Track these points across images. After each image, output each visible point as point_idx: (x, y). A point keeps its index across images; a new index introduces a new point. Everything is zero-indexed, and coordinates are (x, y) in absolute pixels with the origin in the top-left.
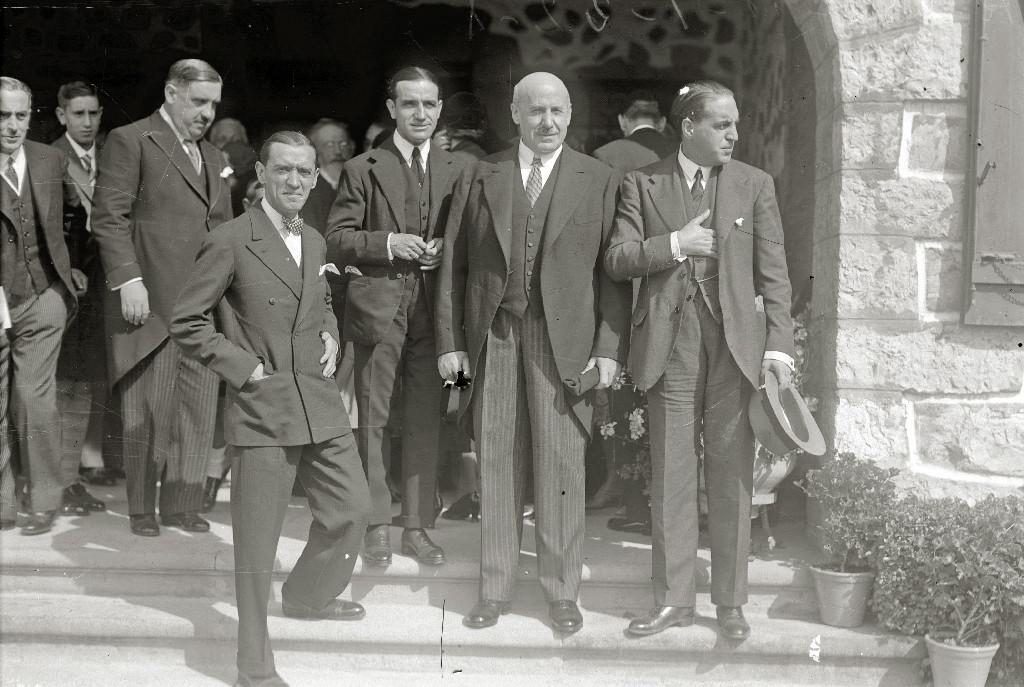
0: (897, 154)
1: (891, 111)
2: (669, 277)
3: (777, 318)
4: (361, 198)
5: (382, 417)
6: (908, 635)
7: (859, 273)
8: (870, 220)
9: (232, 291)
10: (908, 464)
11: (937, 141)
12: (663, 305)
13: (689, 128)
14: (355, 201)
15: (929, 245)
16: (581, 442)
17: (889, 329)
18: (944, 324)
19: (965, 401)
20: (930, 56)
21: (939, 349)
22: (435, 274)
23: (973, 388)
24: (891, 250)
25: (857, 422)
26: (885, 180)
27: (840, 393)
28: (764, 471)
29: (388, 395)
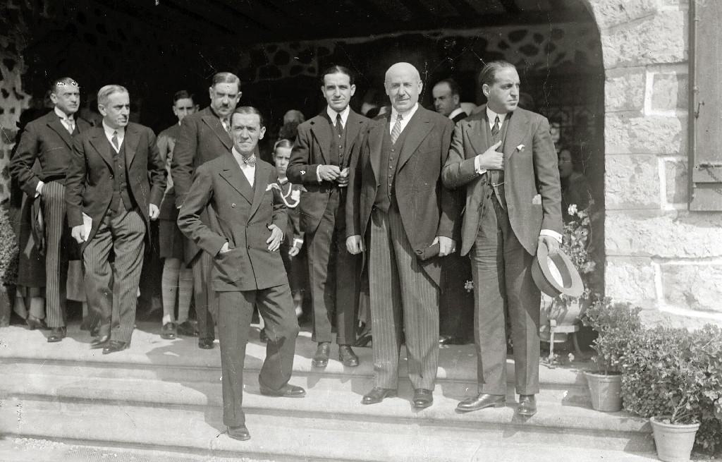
0: (643, 102)
1: (637, 72)
2: (475, 185)
3: (550, 209)
4: (305, 145)
5: (322, 277)
6: (643, 417)
7: (619, 179)
8: (625, 144)
9: (212, 200)
10: (656, 305)
11: (670, 90)
12: (473, 201)
13: (487, 90)
14: (303, 148)
15: (667, 159)
16: (433, 291)
17: (640, 215)
18: (679, 211)
19: (695, 263)
20: (663, 35)
21: (675, 228)
22: (345, 189)
23: (699, 254)
24: (639, 163)
25: (620, 278)
26: (634, 117)
27: (607, 259)
28: (562, 311)
29: (326, 264)
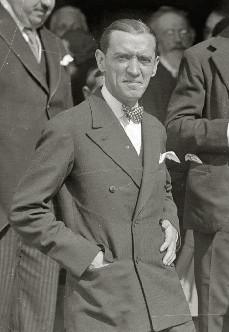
4: (201, 86)
9: (72, 179)
14: (195, 89)
